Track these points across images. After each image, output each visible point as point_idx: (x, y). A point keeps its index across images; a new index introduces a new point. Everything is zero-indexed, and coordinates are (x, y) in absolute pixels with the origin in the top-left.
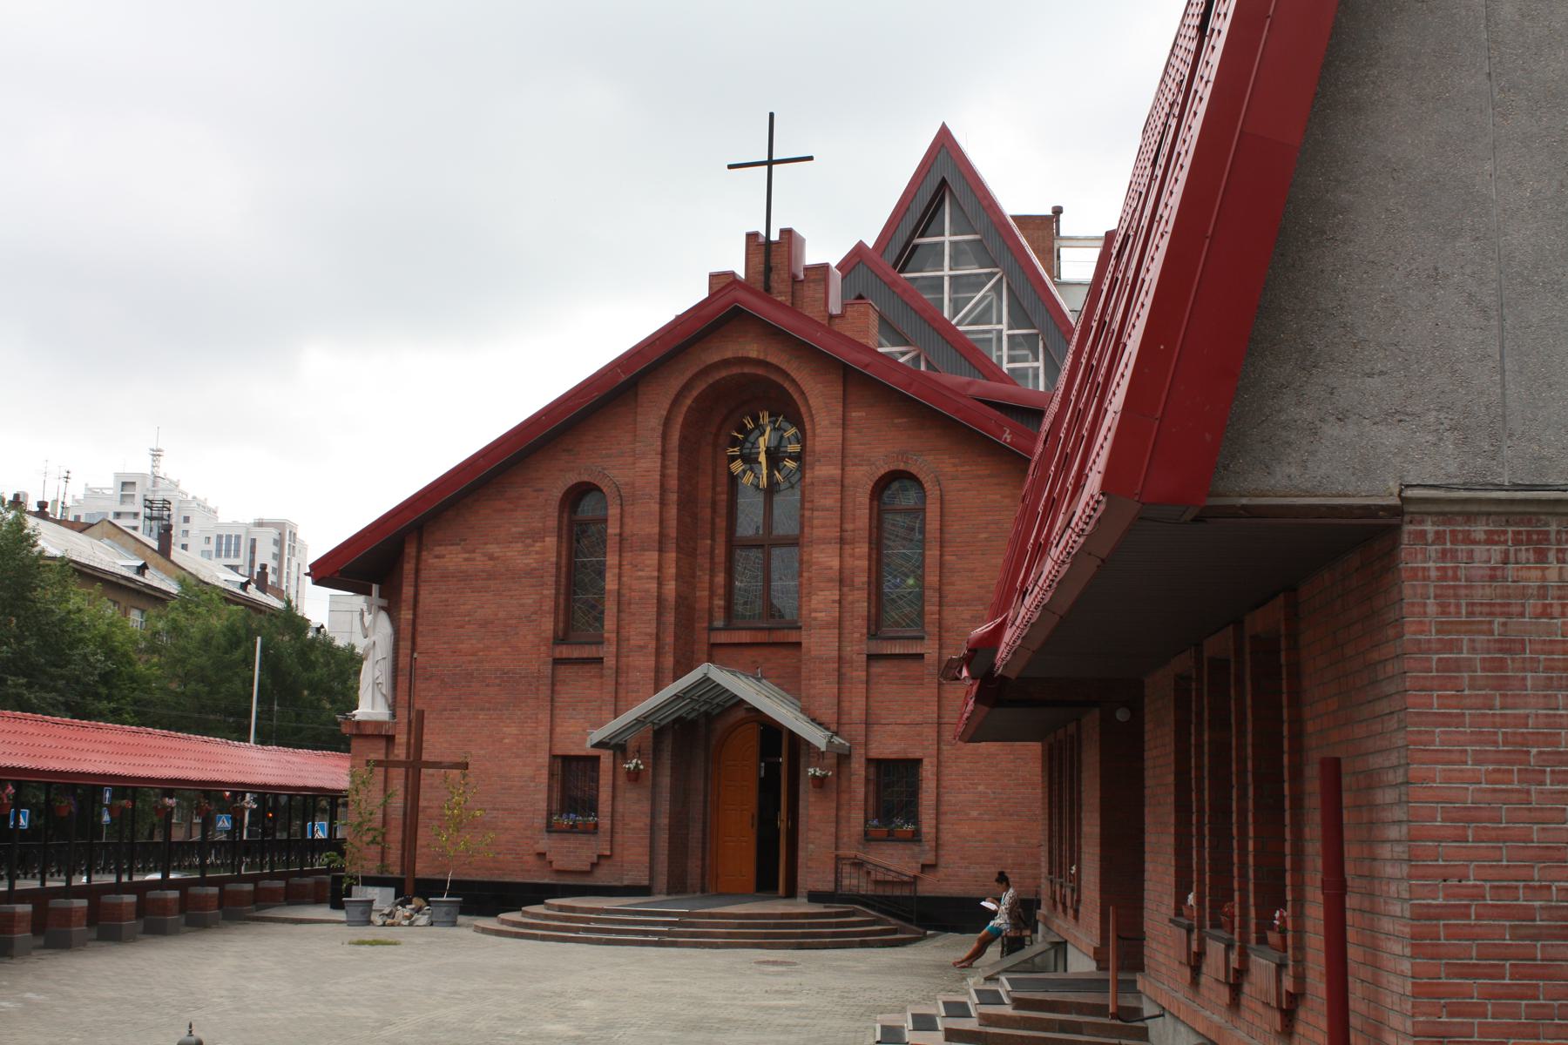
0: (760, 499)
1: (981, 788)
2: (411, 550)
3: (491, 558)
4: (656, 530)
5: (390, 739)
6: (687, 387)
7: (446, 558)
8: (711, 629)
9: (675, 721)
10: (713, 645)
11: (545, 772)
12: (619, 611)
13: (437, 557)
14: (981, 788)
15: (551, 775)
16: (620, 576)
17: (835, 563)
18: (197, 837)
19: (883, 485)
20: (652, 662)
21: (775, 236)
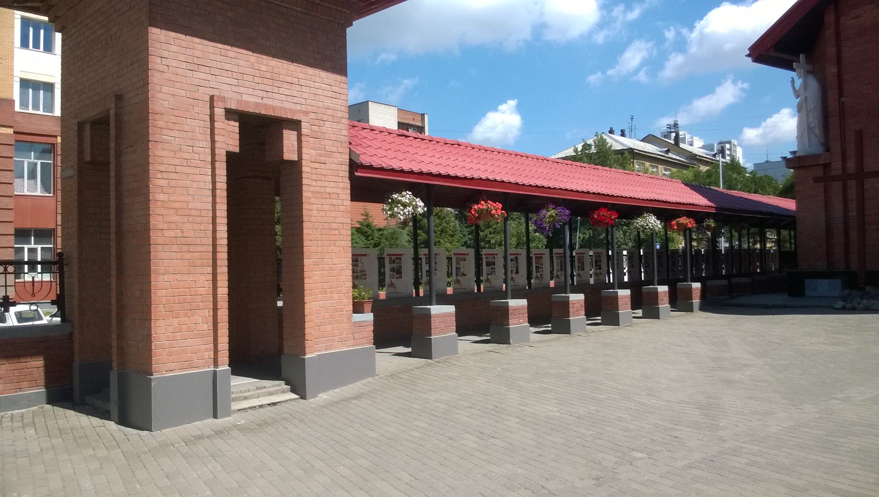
2: (830, 18)
5: (827, 166)
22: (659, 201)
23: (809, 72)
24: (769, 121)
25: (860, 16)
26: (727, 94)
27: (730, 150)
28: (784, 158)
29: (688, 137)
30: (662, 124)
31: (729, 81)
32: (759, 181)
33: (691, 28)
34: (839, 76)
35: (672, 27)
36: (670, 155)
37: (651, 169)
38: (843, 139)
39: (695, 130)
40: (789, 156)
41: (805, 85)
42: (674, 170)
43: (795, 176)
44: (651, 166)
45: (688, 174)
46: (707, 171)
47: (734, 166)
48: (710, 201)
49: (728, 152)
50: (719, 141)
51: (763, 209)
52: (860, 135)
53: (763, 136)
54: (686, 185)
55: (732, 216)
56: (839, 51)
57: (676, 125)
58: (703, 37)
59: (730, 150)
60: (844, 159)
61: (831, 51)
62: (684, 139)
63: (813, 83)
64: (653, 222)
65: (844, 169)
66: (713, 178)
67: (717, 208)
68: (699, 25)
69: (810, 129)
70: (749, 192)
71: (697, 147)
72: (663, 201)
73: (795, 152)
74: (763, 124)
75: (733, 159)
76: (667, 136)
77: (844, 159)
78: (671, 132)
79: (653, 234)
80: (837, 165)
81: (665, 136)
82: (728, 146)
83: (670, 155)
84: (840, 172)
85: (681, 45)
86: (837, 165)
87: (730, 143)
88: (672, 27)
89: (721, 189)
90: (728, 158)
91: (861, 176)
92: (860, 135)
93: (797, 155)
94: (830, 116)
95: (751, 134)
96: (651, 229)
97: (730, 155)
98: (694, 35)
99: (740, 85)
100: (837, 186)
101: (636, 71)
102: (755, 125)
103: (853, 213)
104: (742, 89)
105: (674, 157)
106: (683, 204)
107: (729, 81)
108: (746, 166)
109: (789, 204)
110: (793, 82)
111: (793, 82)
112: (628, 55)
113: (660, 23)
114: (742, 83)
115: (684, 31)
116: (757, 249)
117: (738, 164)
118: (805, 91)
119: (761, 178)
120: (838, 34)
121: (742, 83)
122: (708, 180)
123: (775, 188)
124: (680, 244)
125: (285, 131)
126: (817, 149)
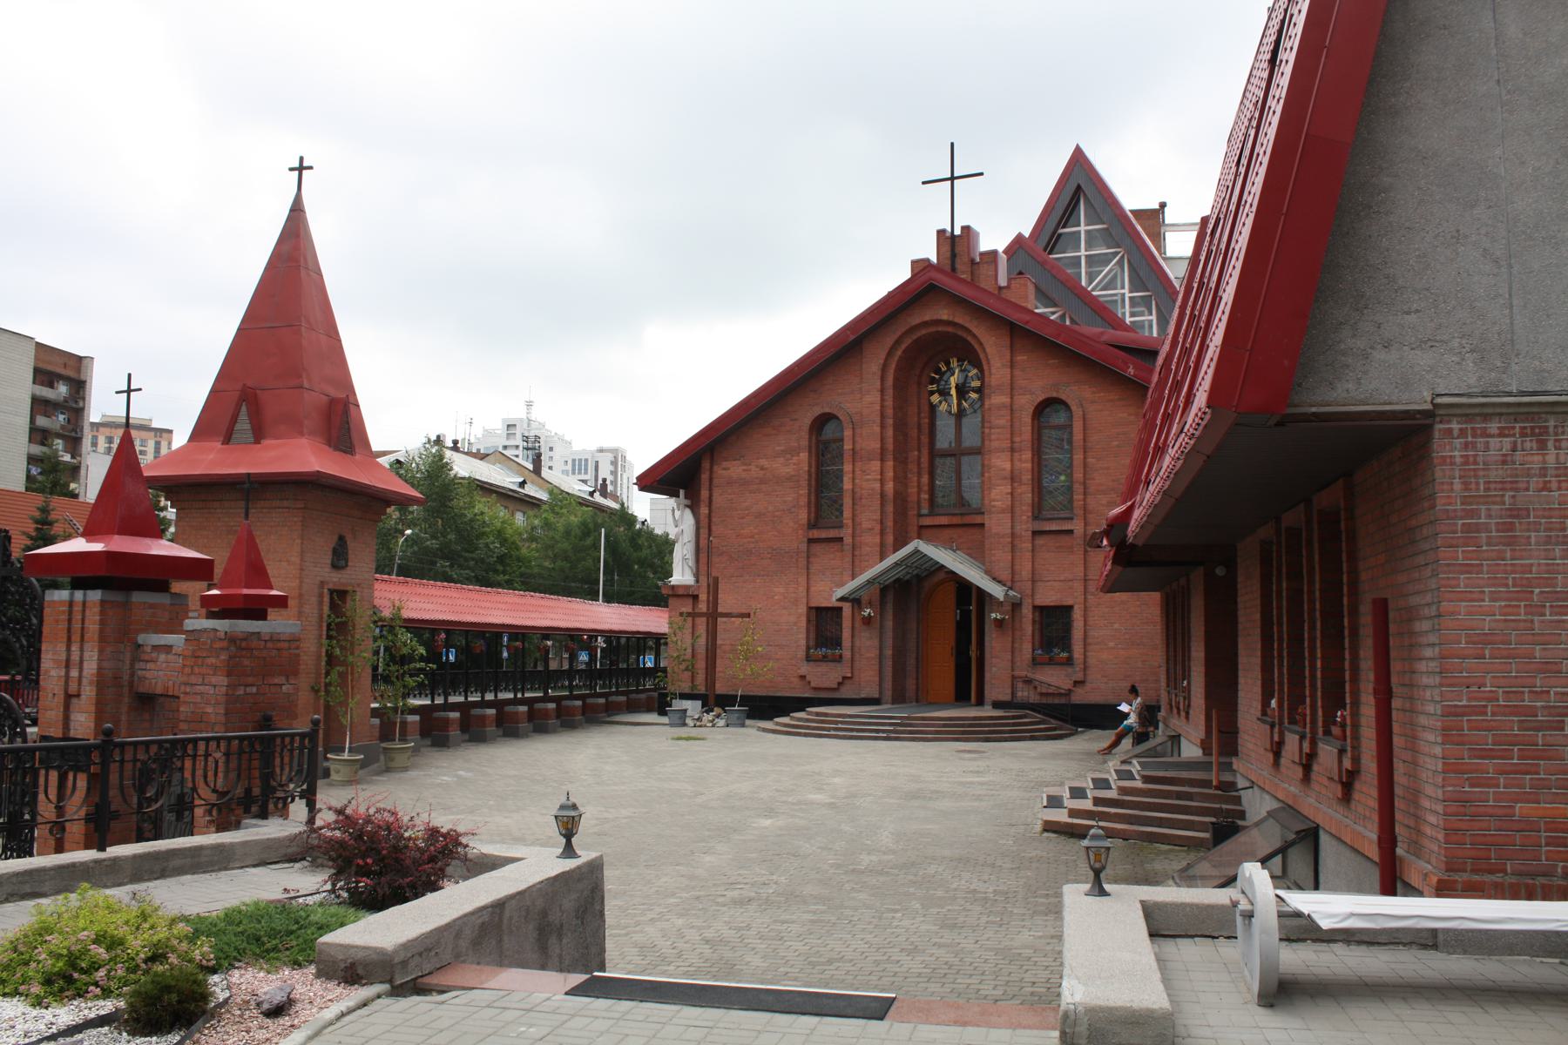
0: (952, 421)
2: (706, 465)
6: (898, 342)
7: (730, 469)
8: (920, 515)
10: (921, 527)
11: (804, 619)
15: (809, 621)
17: (1008, 466)
20: (878, 540)
21: (957, 232)
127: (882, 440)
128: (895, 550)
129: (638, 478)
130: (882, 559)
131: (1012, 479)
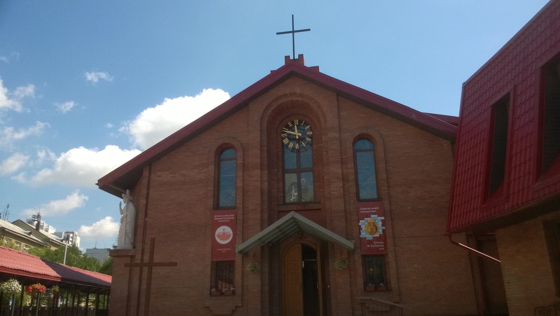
0: (294, 155)
1: (416, 266)
2: (146, 173)
3: (184, 176)
4: (259, 161)
5: (132, 257)
6: (269, 105)
7: (161, 175)
8: (279, 205)
9: (269, 243)
10: (279, 212)
11: (209, 268)
12: (243, 195)
13: (158, 176)
14: (416, 266)
15: (212, 269)
16: (243, 180)
17: (340, 171)
18: (101, 296)
19: (361, 137)
20: (259, 216)
21: (297, 57)
22: (23, 271)
23: (130, 201)
24: (98, 223)
25: (161, 176)
26: (74, 201)
27: (72, 238)
28: (109, 249)
29: (45, 226)
30: (28, 214)
31: (76, 194)
32: (88, 261)
33: (58, 155)
34: (147, 205)
35: (44, 151)
36: (32, 236)
37: (16, 245)
38: (144, 242)
39: (52, 221)
40: (112, 248)
41: (127, 207)
42: (32, 247)
43: (112, 261)
44: (16, 242)
45: (42, 251)
46: (56, 250)
47: (74, 249)
48: (58, 273)
49: (71, 239)
50: (66, 231)
51: (91, 281)
52: (153, 240)
53: (93, 231)
54: (43, 260)
55: (72, 285)
56: (148, 194)
57: (39, 216)
58: (66, 163)
59: (72, 238)
60: (143, 254)
61: (144, 191)
62: (43, 226)
63: (132, 207)
64: (16, 286)
65: (142, 259)
66: (59, 256)
67: (62, 279)
68: (63, 155)
69: (126, 233)
70: (81, 268)
71: (50, 232)
72: (26, 271)
73: (116, 247)
74: (94, 224)
75: (74, 245)
76: (31, 222)
77: (143, 254)
78: (35, 221)
79: (14, 293)
80: (138, 257)
81: (29, 223)
82: (71, 235)
83: (32, 236)
84: (139, 262)
85: (50, 165)
86: (138, 257)
87: (73, 233)
88: (44, 151)
89: (64, 265)
90: (70, 243)
91: (151, 265)
92: (153, 240)
93: (117, 248)
94: (139, 227)
95: (85, 229)
96: (14, 291)
97: (72, 241)
98: (60, 160)
99: (83, 197)
100: (137, 270)
101: (17, 173)
102: (87, 225)
103: (144, 287)
104: (84, 200)
105: (34, 238)
106: (40, 274)
107: (76, 194)
108: (81, 249)
109: (107, 279)
110: (121, 204)
111: (121, 204)
112: (10, 161)
113: (38, 146)
114: (85, 196)
115: (52, 155)
116: (81, 307)
117: (77, 248)
118: (127, 210)
119: (89, 259)
120: (149, 183)
121: (85, 196)
122: (55, 257)
123: (98, 267)
124: (28, 302)
125: (454, 111)
126: (129, 246)
127: (261, 158)
128: (269, 225)
129: (99, 181)
130: (262, 229)
131: (343, 180)
